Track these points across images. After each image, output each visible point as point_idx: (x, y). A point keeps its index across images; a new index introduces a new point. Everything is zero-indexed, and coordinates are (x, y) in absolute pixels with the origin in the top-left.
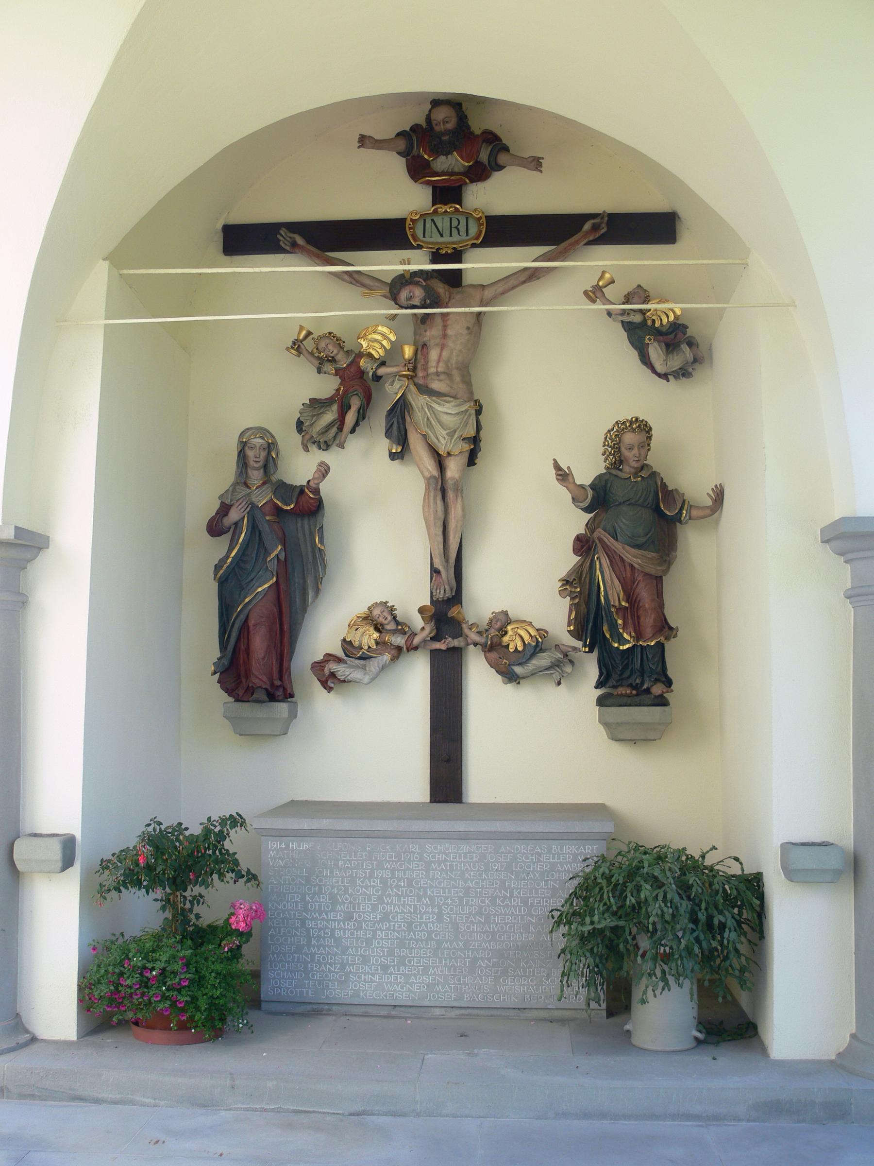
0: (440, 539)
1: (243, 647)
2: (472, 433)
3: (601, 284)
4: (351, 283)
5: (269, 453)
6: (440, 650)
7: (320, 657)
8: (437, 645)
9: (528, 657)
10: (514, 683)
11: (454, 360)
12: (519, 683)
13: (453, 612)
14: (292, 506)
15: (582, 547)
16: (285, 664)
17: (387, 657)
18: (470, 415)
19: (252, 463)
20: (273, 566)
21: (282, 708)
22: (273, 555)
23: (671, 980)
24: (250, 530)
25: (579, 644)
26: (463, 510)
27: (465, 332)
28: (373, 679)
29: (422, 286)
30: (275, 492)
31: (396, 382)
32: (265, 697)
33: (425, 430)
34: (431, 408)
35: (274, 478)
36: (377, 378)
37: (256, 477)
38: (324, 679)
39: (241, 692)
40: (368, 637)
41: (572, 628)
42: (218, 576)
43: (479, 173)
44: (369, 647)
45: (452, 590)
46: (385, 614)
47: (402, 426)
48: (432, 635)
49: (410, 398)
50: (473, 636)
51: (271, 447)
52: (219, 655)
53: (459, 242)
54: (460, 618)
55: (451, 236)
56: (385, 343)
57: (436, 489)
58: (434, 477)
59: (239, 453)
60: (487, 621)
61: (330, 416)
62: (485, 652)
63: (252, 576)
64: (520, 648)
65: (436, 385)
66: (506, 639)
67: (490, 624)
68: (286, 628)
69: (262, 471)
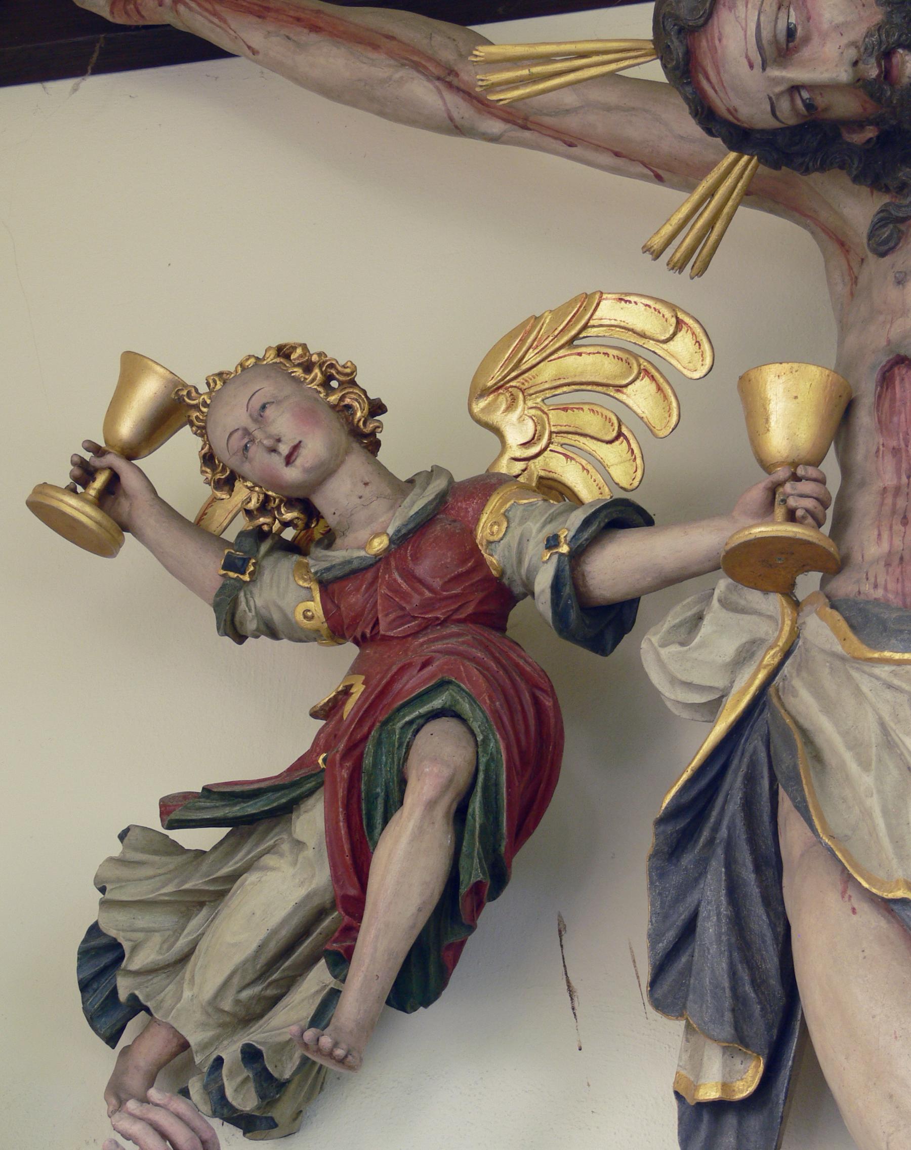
4: (457, 129)
23: (88, 456)
31: (715, 614)
36: (604, 623)
49: (803, 701)
56: (640, 397)
61: (283, 884)
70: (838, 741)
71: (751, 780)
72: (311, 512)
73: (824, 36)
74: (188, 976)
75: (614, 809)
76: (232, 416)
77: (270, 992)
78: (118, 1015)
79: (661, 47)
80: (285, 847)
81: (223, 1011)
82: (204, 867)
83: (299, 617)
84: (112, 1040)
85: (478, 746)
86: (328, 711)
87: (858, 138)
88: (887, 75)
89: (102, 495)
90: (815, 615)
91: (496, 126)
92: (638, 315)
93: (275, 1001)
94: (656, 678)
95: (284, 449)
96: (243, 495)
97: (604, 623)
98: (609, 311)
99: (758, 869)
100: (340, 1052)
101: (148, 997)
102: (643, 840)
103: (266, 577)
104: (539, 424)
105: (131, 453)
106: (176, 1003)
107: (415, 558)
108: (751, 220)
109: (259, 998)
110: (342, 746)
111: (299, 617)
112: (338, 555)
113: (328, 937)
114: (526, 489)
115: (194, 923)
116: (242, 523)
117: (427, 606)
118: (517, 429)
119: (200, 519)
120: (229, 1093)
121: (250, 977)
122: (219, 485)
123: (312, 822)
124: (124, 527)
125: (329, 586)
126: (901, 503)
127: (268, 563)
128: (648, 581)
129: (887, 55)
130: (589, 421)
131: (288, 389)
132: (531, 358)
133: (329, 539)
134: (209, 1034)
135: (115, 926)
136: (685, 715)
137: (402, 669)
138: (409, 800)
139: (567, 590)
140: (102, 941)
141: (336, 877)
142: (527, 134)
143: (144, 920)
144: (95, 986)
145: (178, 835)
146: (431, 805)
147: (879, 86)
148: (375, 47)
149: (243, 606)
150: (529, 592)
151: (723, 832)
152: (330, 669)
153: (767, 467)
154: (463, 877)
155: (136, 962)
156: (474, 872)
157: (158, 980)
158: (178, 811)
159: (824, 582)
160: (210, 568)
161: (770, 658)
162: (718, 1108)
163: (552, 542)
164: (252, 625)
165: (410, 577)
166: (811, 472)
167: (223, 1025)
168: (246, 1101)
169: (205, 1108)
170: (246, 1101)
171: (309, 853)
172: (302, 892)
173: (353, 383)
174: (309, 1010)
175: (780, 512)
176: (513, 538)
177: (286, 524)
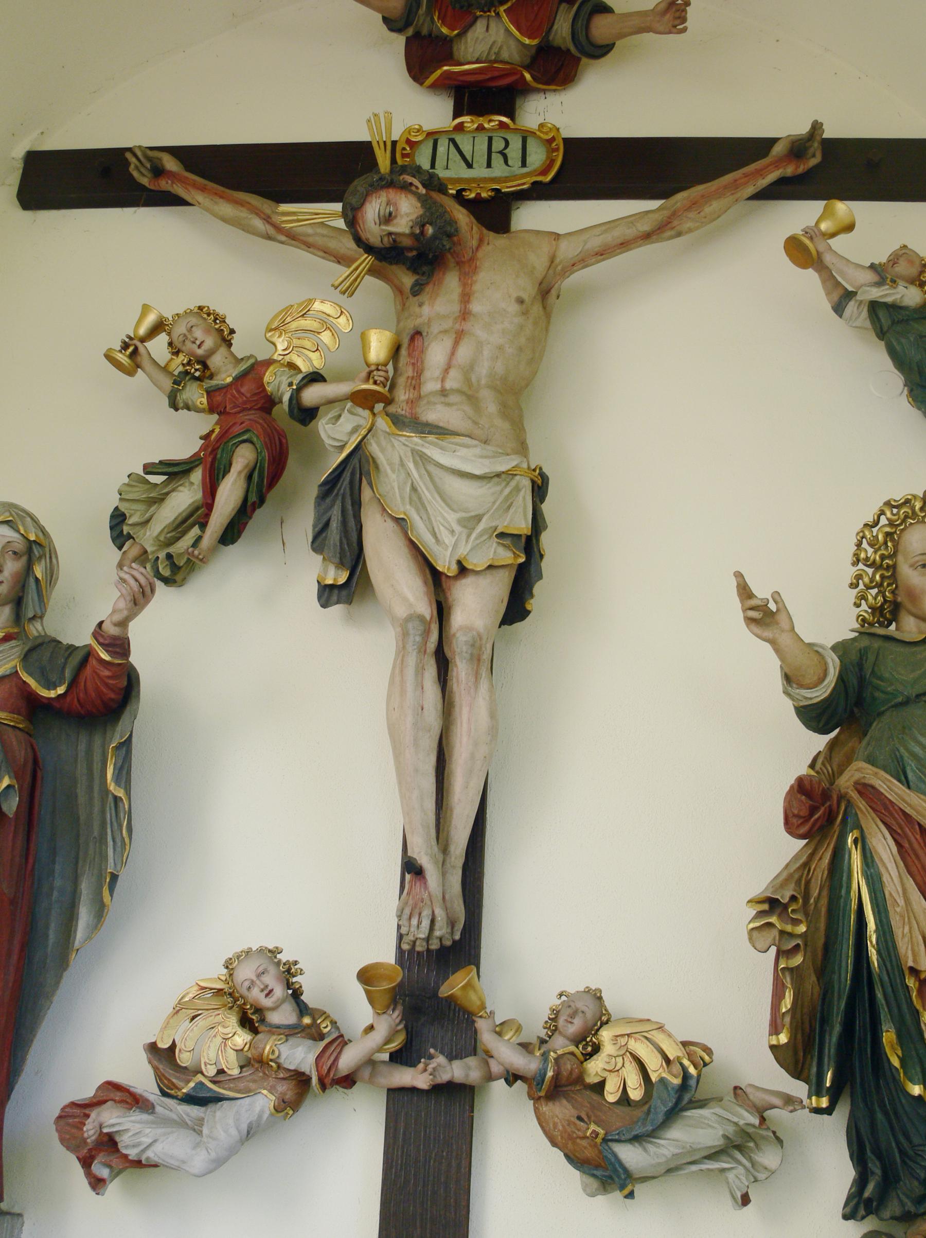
0: (429, 783)
2: (522, 525)
3: (823, 226)
4: (269, 238)
5: (29, 568)
6: (413, 1090)
7: (88, 1092)
8: (407, 1077)
9: (661, 1117)
10: (617, 1195)
11: (483, 370)
12: (631, 1195)
13: (454, 985)
14: (61, 690)
15: (813, 810)
17: (263, 1102)
18: (517, 489)
25: (799, 1089)
26: (493, 715)
27: (514, 308)
28: (219, 1163)
29: (419, 197)
30: (25, 658)
33: (401, 508)
34: (422, 459)
35: (34, 630)
36: (306, 415)
40: (217, 1044)
41: (783, 1038)
43: (556, 67)
44: (221, 1072)
45: (452, 924)
46: (270, 980)
47: (352, 523)
48: (394, 1046)
49: (374, 448)
50: (507, 1054)
53: (506, 179)
54: (473, 1000)
55: (489, 165)
56: (326, 337)
57: (422, 650)
58: (421, 618)
60: (545, 1014)
61: (185, 497)
62: (536, 1099)
64: (635, 1094)
65: (434, 414)
66: (595, 1068)
67: (553, 1025)
70: (385, 462)
71: (353, 474)
72: (205, 366)
73: (402, 217)
75: (304, 482)
76: (180, 329)
77: (178, 535)
78: (122, 539)
79: (344, 214)
80: (187, 484)
83: (198, 403)
84: (120, 548)
85: (258, 453)
86: (206, 437)
87: (411, 254)
88: (422, 233)
89: (131, 355)
91: (283, 238)
92: (328, 308)
93: (178, 539)
94: (323, 435)
95: (198, 342)
96: (182, 358)
97: (306, 415)
98: (317, 306)
99: (352, 505)
100: (201, 557)
102: (313, 492)
103: (188, 388)
104: (289, 343)
105: (143, 340)
107: (241, 386)
108: (369, 280)
110: (210, 450)
111: (198, 403)
112: (214, 382)
113: (199, 517)
114: (283, 365)
115: (153, 508)
116: (181, 369)
117: (245, 403)
118: (281, 345)
119: (165, 367)
120: (160, 569)
121: (171, 528)
122: (173, 354)
123: (197, 476)
124: (138, 366)
125: (209, 393)
126: (414, 382)
127: (189, 384)
128: (323, 401)
129: (423, 226)
130: (307, 344)
131: (201, 322)
132: (288, 320)
133: (211, 377)
134: (155, 548)
135: (124, 507)
136: (332, 450)
137: (235, 424)
138: (232, 470)
139: (294, 402)
142: (293, 242)
143: (135, 506)
145: (149, 477)
146: (240, 472)
147: (418, 237)
148: (242, 205)
149: (178, 398)
150: (281, 402)
151: (342, 491)
152: (207, 423)
153: (368, 365)
154: (249, 499)
156: (253, 498)
157: (138, 528)
158: (149, 469)
159: (384, 408)
160: (168, 384)
161: (364, 432)
162: (332, 587)
163: (290, 384)
164: (181, 405)
165: (239, 392)
166: (384, 368)
168: (166, 572)
169: (152, 574)
170: (166, 572)
171: (195, 487)
173: (224, 322)
174: (191, 542)
175: (371, 381)
176: (276, 382)
177: (196, 370)
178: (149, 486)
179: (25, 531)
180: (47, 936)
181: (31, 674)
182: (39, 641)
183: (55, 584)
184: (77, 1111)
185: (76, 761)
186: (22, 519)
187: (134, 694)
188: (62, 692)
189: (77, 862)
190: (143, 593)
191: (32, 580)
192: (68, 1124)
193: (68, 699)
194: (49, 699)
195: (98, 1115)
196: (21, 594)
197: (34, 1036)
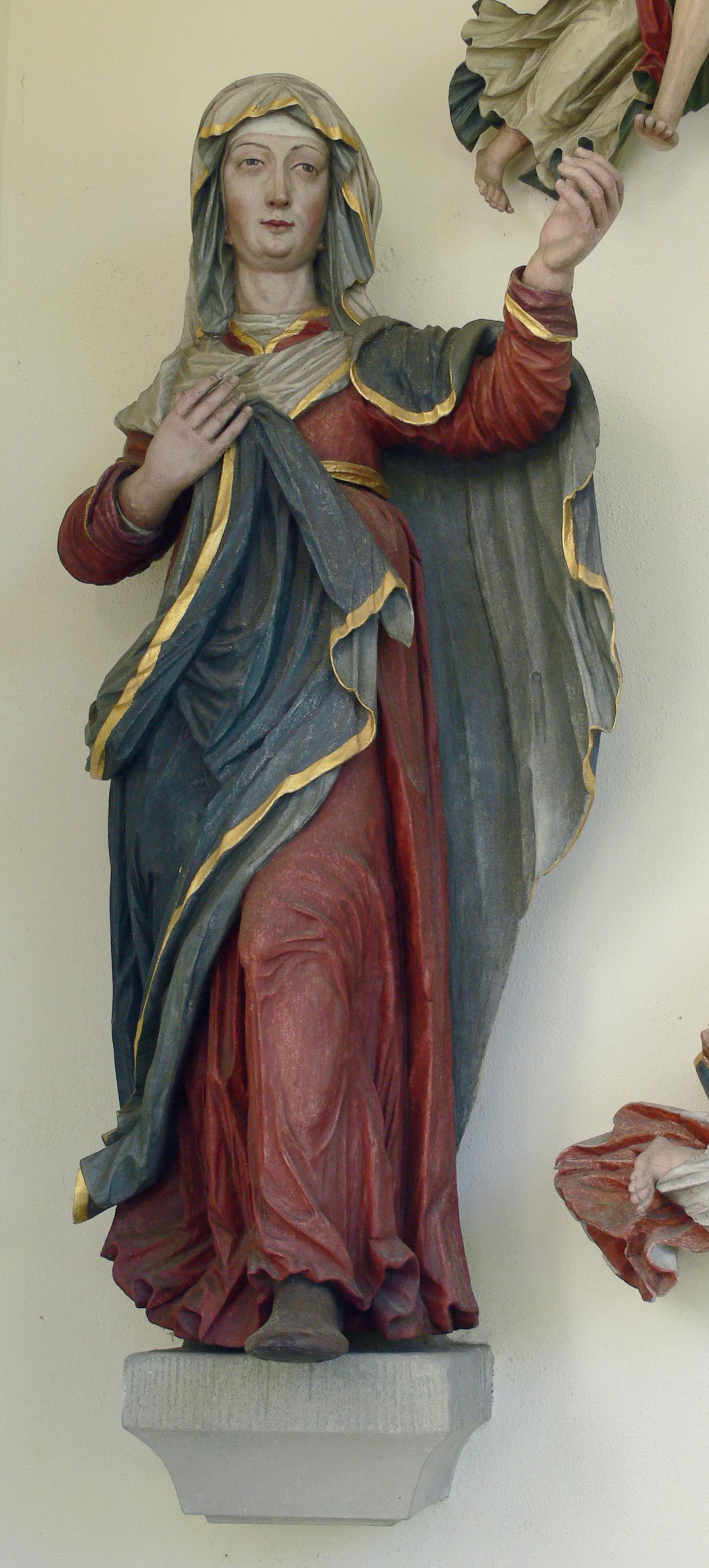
1: (215, 1073)
5: (332, 195)
7: (597, 1125)
14: (444, 409)
16: (429, 1162)
19: (255, 237)
20: (359, 670)
21: (414, 1382)
22: (356, 619)
24: (246, 517)
32: (331, 1332)
35: (364, 306)
37: (276, 299)
38: (625, 1231)
39: (207, 1302)
42: (104, 734)
51: (337, 159)
52: (111, 1124)
59: (201, 197)
63: (257, 726)
68: (428, 977)
69: (302, 278)
74: (529, 97)
77: (586, 106)
78: (476, 128)
81: (554, 120)
82: (536, 23)
84: (470, 147)
90: (643, 137)
101: (503, 113)
106: (523, 115)
109: (578, 110)
121: (574, 96)
134: (545, 136)
135: (477, 66)
140: (466, 77)
141: (642, 20)
144: (460, 109)
155: (492, 90)
157: (506, 102)
167: (551, 131)
172: (615, 34)
178: (517, 20)
179: (322, 124)
180: (472, 859)
181: (376, 388)
182: (375, 328)
183: (378, 219)
184: (587, 1161)
185: (470, 541)
186: (312, 100)
187: (582, 400)
188: (447, 412)
189: (506, 721)
190: (606, 197)
191: (341, 218)
192: (584, 1184)
193: (457, 425)
194: (424, 428)
195: (649, 1161)
196: (321, 246)
197: (487, 1036)
